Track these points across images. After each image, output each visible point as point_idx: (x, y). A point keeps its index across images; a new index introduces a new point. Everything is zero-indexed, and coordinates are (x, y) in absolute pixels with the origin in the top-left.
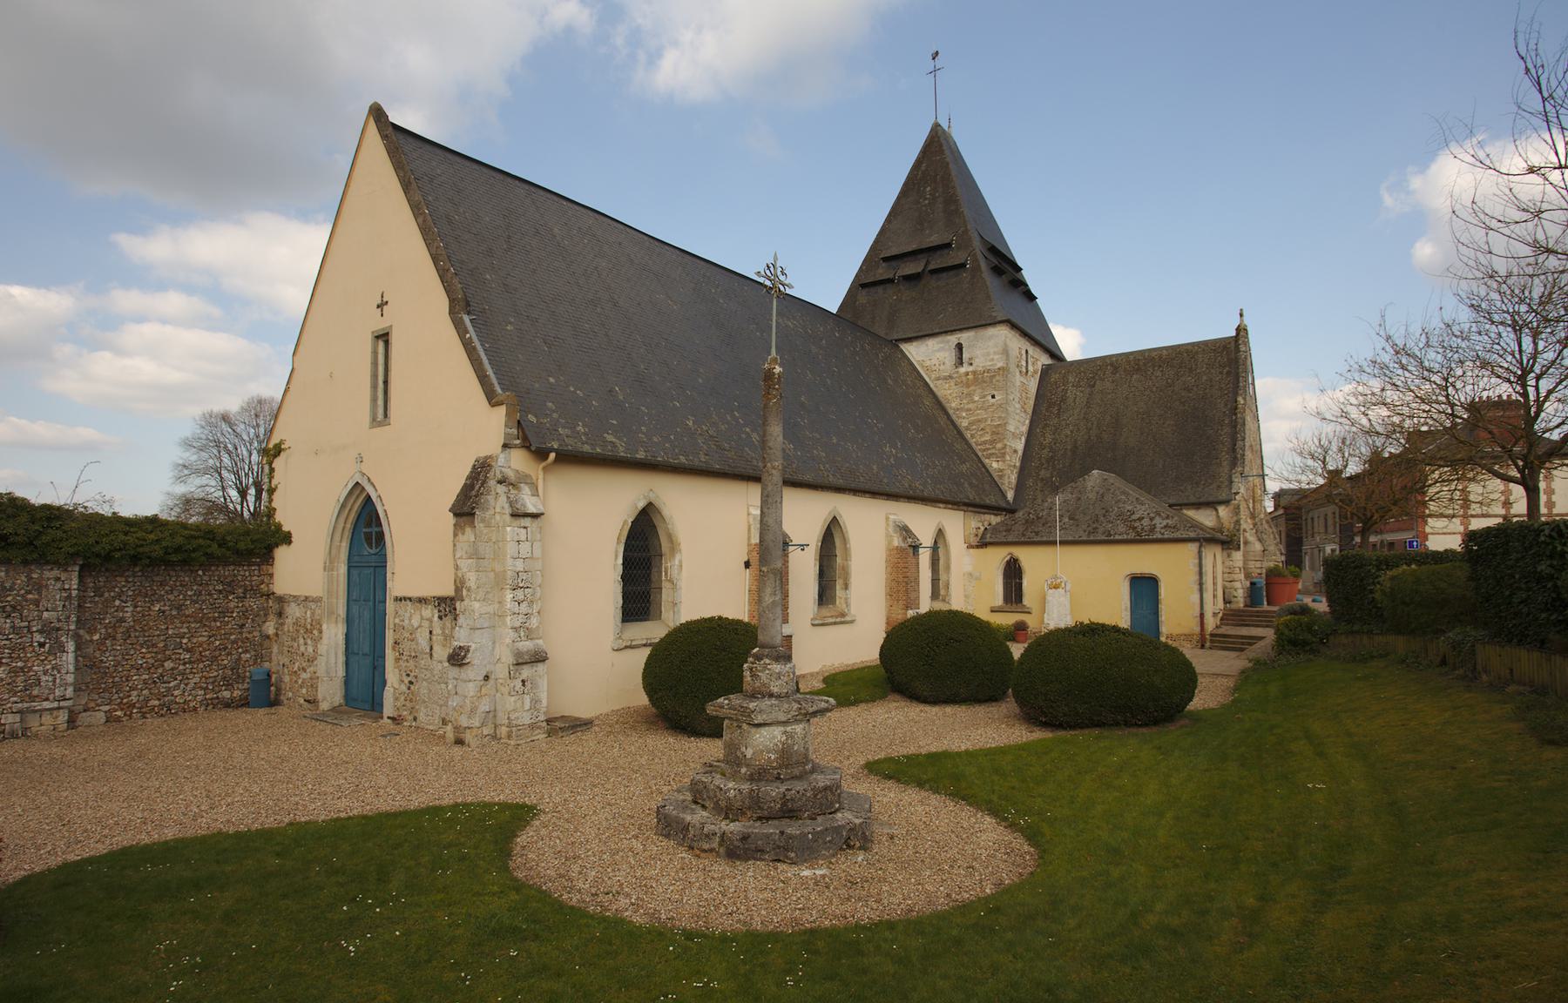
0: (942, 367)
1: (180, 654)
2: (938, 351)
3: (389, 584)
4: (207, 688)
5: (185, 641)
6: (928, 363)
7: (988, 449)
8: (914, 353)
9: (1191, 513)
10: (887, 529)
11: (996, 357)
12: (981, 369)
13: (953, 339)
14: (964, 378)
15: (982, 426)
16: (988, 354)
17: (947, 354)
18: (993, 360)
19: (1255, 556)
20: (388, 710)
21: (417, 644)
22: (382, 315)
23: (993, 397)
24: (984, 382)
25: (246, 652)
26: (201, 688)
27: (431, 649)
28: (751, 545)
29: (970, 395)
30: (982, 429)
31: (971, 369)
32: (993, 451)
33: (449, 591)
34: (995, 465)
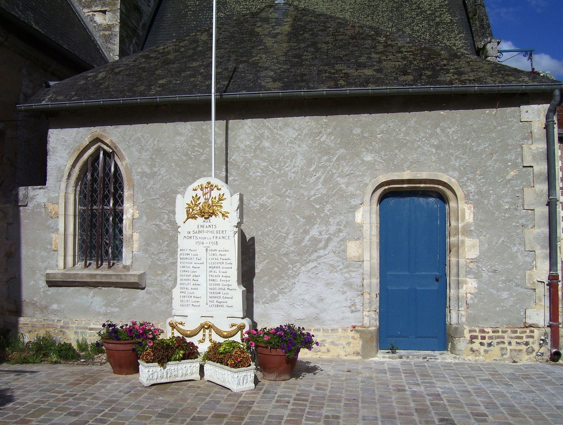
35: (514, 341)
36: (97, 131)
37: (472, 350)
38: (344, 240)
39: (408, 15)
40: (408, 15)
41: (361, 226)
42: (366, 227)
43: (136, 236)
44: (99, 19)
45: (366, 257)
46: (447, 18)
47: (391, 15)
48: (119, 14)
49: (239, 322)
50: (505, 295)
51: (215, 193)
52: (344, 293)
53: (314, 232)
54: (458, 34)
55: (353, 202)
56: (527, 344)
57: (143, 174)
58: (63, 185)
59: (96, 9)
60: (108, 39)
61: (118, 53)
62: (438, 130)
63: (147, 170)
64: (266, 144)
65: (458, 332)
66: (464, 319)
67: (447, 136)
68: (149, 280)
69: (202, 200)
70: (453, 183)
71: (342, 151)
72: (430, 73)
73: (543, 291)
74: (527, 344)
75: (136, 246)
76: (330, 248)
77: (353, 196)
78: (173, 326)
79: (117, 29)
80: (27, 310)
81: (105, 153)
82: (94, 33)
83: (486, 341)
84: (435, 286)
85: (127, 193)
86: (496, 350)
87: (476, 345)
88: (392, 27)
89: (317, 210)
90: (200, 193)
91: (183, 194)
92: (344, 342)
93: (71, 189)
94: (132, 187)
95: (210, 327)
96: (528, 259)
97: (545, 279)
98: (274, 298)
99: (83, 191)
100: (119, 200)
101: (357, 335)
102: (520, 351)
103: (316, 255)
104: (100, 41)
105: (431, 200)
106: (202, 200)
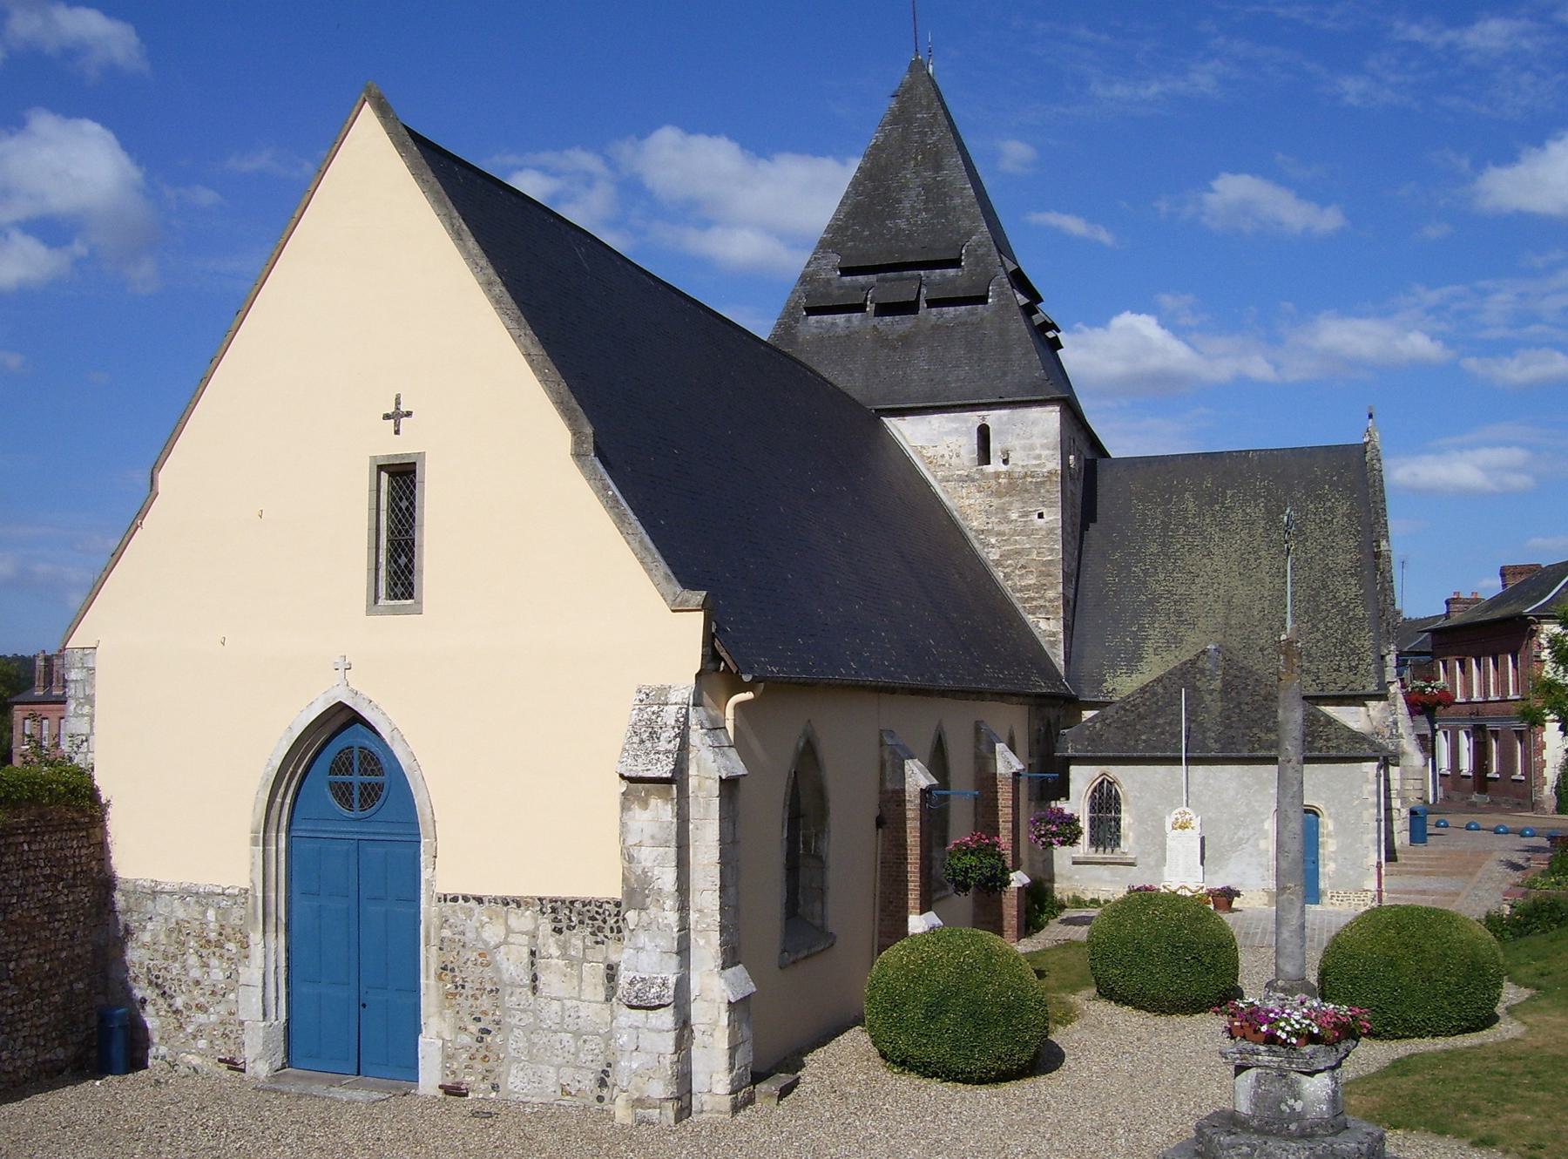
0: (954, 461)
1: (7, 988)
2: (949, 433)
3: (425, 874)
4: (38, 1045)
5: (12, 966)
6: (929, 453)
7: (1033, 599)
8: (907, 434)
9: (1330, 710)
10: (976, 747)
11: (1045, 453)
12: (1019, 469)
13: (973, 419)
14: (993, 482)
15: (1022, 562)
16: (1032, 448)
17: (963, 440)
18: (1039, 457)
19: (1414, 773)
20: (430, 1077)
21: (498, 970)
22: (397, 432)
23: (1041, 516)
24: (1026, 491)
25: (79, 979)
26: (32, 1045)
27: (535, 978)
28: (886, 792)
29: (1003, 510)
30: (1023, 567)
31: (1003, 468)
32: (1041, 602)
33: (612, 889)
34: (1043, 625)
35: (1356, 899)
36: (1104, 768)
37: (1332, 904)
38: (1257, 839)
39: (1323, 607)
40: (1323, 607)
41: (1268, 830)
42: (1271, 831)
43: (1131, 834)
44: (1043, 625)
45: (1271, 849)
46: (1360, 612)
47: (1307, 605)
48: (1062, 623)
49: (1201, 885)
50: (1351, 873)
51: (1187, 817)
52: (1257, 869)
53: (1240, 834)
54: (1368, 633)
55: (1263, 817)
56: (1363, 900)
57: (1135, 797)
58: (1082, 802)
59: (1040, 616)
60: (1053, 644)
61: (1063, 658)
62: (1314, 776)
63: (1138, 795)
64: (1211, 781)
65: (1325, 893)
66: (1327, 886)
67: (1319, 779)
68: (1138, 862)
69: (1180, 820)
70: (1321, 807)
71: (1257, 787)
72: (1310, 739)
73: (1374, 870)
74: (1363, 900)
75: (1131, 840)
76: (1250, 843)
77: (1262, 813)
78: (1164, 887)
79: (1061, 636)
80: (1056, 879)
81: (1108, 781)
82: (1040, 639)
83: (1340, 899)
84: (1312, 866)
85: (1123, 808)
86: (1345, 904)
87: (1334, 901)
88: (1308, 622)
89: (1242, 821)
90: (1179, 816)
91: (1170, 814)
92: (1258, 898)
93: (1086, 804)
94: (1127, 804)
95: (1185, 887)
96: (1366, 852)
97: (1375, 864)
98: (1216, 872)
99: (392, 494)
100: (1118, 811)
101: (1265, 894)
102: (1360, 905)
103: (1240, 847)
104: (1046, 647)
105: (1310, 815)
106: (1180, 820)
